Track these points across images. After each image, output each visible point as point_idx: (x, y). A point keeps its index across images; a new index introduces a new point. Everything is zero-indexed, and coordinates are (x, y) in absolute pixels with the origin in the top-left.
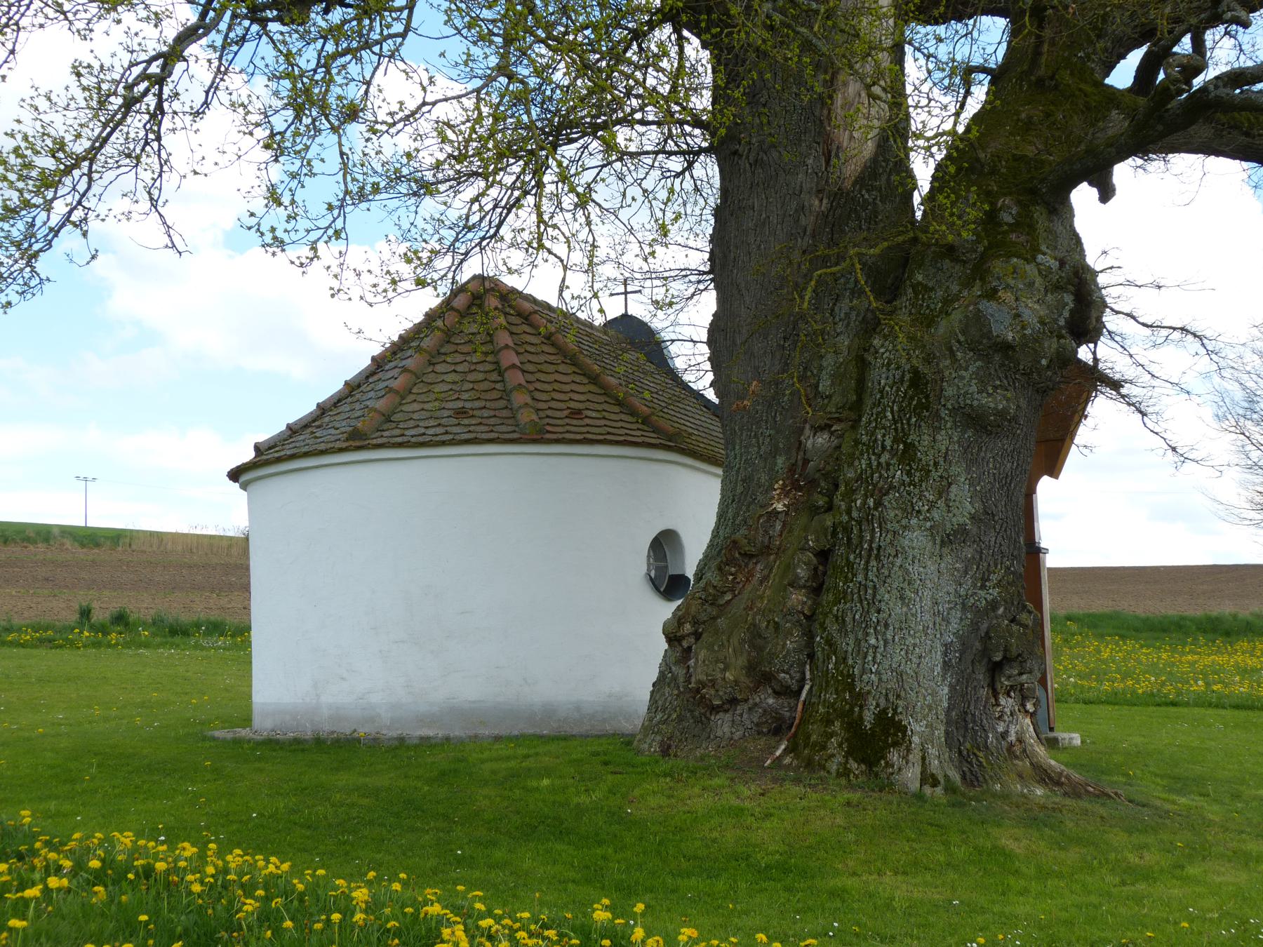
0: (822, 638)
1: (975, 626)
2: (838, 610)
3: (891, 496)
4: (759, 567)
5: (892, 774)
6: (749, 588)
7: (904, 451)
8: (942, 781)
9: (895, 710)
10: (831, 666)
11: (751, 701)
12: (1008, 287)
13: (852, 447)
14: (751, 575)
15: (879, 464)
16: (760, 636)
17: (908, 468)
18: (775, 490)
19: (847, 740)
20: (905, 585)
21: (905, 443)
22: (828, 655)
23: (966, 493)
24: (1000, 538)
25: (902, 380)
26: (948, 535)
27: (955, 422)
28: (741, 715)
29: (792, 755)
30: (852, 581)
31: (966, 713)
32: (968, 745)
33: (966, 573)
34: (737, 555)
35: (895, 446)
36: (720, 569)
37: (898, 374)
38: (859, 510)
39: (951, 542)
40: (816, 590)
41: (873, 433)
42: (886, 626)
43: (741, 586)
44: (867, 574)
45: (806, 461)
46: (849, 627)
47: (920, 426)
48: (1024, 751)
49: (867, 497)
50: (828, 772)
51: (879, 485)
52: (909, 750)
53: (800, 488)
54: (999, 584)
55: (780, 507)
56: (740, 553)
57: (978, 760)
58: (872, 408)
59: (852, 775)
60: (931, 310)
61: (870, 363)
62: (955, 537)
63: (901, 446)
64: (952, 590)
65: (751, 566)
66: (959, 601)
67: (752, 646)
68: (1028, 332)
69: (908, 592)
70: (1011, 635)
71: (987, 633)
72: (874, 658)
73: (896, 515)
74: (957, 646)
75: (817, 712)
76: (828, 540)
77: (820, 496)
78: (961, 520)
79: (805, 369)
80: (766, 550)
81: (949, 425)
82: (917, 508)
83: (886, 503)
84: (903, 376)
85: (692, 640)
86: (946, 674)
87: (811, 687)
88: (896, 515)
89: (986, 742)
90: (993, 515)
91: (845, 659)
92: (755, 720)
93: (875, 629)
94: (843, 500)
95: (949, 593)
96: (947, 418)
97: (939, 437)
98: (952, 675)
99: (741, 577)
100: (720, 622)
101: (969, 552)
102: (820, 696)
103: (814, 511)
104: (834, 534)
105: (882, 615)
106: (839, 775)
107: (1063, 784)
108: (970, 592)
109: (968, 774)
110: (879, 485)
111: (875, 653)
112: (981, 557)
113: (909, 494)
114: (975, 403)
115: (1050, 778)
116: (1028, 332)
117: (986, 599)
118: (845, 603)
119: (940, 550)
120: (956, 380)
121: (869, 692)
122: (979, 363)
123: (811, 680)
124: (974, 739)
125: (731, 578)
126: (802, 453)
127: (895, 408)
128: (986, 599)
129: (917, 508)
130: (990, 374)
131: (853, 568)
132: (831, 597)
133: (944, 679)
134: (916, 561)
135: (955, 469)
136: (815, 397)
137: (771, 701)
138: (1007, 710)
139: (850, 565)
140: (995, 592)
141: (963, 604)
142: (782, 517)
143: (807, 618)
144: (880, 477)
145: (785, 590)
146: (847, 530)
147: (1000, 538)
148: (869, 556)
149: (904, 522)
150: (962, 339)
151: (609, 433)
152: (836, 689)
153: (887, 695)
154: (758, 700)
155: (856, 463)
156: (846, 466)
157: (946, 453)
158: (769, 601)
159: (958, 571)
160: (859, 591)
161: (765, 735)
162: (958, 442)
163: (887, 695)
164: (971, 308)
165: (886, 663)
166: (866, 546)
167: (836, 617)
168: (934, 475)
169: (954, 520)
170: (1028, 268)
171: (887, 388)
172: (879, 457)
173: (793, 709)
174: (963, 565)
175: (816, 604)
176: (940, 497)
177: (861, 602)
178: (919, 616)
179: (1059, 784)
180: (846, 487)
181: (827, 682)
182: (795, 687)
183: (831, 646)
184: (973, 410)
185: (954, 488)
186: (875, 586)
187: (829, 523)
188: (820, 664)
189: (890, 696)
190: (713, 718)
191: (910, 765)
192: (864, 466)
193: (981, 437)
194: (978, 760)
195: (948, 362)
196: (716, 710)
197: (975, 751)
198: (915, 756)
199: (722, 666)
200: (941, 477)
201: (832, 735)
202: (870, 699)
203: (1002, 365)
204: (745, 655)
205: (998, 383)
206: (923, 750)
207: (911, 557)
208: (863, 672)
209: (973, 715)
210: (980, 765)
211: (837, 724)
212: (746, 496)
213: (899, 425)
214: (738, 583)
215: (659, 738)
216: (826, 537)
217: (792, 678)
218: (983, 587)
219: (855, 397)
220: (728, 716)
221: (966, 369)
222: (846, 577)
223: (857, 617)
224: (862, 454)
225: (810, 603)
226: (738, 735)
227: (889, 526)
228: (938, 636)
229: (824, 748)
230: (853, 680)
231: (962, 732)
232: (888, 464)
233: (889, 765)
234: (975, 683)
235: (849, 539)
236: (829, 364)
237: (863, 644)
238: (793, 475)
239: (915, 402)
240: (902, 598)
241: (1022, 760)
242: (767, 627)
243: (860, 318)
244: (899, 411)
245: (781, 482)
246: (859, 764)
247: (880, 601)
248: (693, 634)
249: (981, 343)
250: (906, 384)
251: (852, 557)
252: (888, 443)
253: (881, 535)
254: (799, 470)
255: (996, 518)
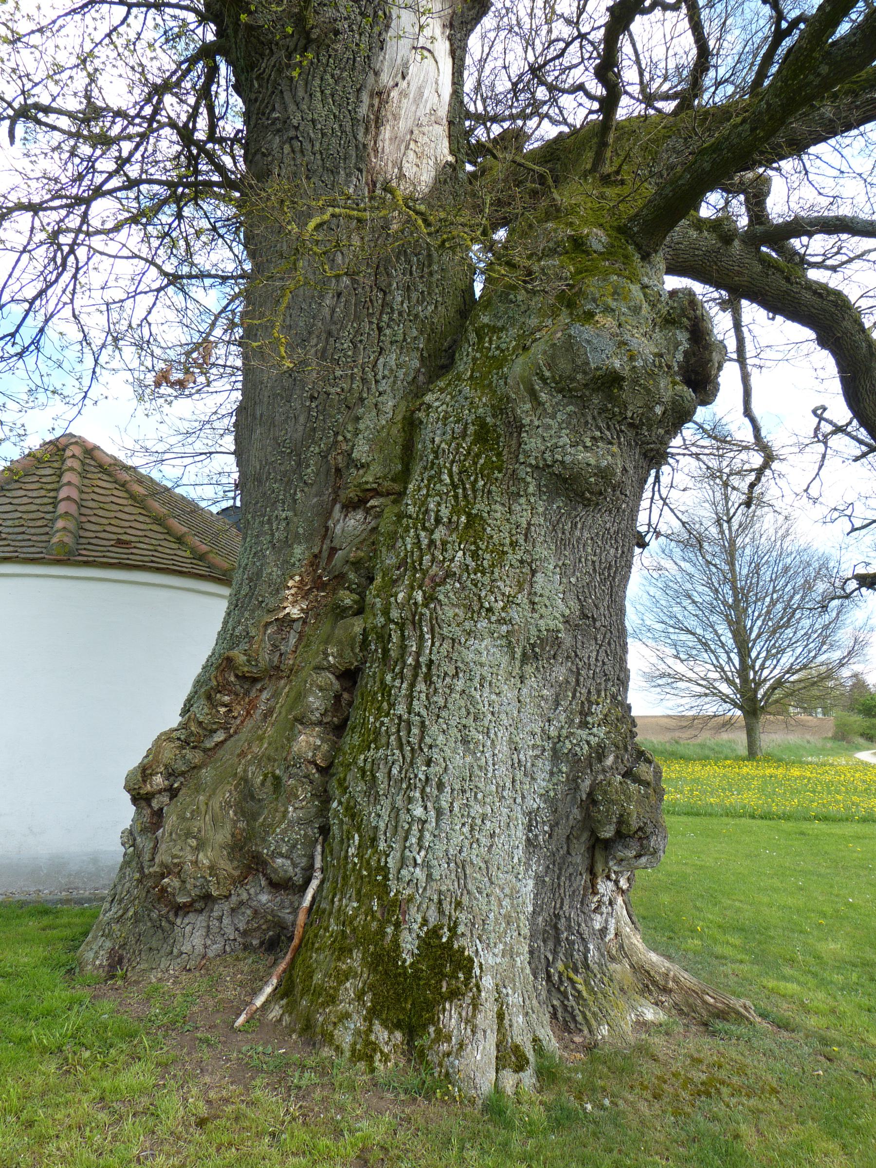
0: (340, 803)
1: (573, 782)
2: (365, 760)
3: (448, 586)
4: (265, 695)
5: (448, 1054)
6: (249, 724)
7: (468, 525)
8: (531, 1055)
9: (453, 929)
10: (352, 851)
11: (234, 899)
12: (608, 310)
13: (394, 523)
14: (252, 706)
15: (432, 542)
16: (253, 797)
17: (473, 548)
18: (289, 588)
19: (372, 987)
20: (470, 721)
21: (469, 515)
22: (349, 832)
23: (557, 586)
24: (602, 655)
25: (464, 435)
26: (533, 646)
27: (539, 486)
28: (220, 919)
29: (283, 1002)
30: (387, 714)
31: (557, 916)
32: (560, 966)
33: (557, 704)
34: (232, 679)
35: (455, 518)
36: (209, 698)
37: (458, 429)
38: (401, 607)
39: (536, 657)
40: (339, 729)
41: (424, 503)
42: (440, 786)
43: (238, 722)
44: (411, 704)
45: (333, 550)
46: (382, 787)
47: (490, 492)
48: (621, 947)
49: (412, 588)
50: (338, 1049)
51: (432, 572)
52: (475, 1005)
53: (322, 586)
54: (605, 721)
55: (295, 612)
56: (237, 676)
57: (574, 988)
58: (422, 474)
59: (378, 1056)
60: (502, 351)
61: (421, 422)
62: (543, 649)
63: (463, 519)
64: (538, 730)
65: (253, 694)
66: (548, 746)
67: (242, 812)
68: (639, 363)
69: (474, 732)
70: (629, 798)
71: (590, 794)
72: (420, 839)
73: (456, 615)
74: (545, 814)
75: (326, 929)
76: (355, 654)
77: (347, 592)
78: (552, 624)
79: (336, 434)
80: (275, 672)
81: (531, 489)
82: (487, 605)
83: (441, 597)
84: (465, 428)
85: (166, 799)
86: (529, 859)
87: (322, 882)
88: (456, 615)
89: (586, 958)
90: (594, 620)
91: (374, 840)
92: (242, 926)
93: (423, 791)
94: (378, 596)
95: (533, 734)
96: (529, 479)
97: (516, 508)
98: (539, 859)
99: (238, 710)
100: (206, 774)
101: (560, 672)
102: (333, 902)
103: (340, 613)
104: (365, 644)
105: (434, 769)
106: (356, 1056)
107: (671, 991)
108: (564, 732)
109: (560, 1010)
110: (432, 572)
111: (421, 831)
112: (577, 681)
113: (476, 585)
114: (568, 459)
115: (655, 983)
116: (639, 363)
117: (588, 743)
118: (377, 748)
119: (520, 668)
120: (540, 430)
121: (410, 899)
122: (570, 408)
123: (322, 870)
124: (569, 955)
125: (223, 710)
126: (327, 542)
127: (455, 469)
128: (588, 743)
129: (487, 605)
130: (587, 423)
131: (390, 695)
132: (356, 739)
133: (528, 866)
134: (486, 685)
135: (542, 551)
136: (347, 467)
137: (264, 898)
138: (606, 899)
139: (385, 689)
140: (601, 731)
141: (554, 750)
142: (298, 626)
143: (325, 771)
144: (433, 561)
145: (292, 728)
146: (384, 638)
147: (602, 655)
148: (415, 676)
149: (468, 625)
150: (547, 374)
151: (152, 562)
152: (359, 892)
153: (440, 902)
154: (245, 896)
155: (399, 543)
156: (384, 550)
157: (528, 529)
158: (270, 744)
159: (546, 700)
160: (399, 731)
161: (254, 950)
162: (544, 514)
163: (440, 902)
164: (559, 335)
165: (440, 848)
166: (410, 661)
167: (363, 771)
168: (513, 558)
169: (541, 622)
170: (632, 287)
171: (443, 445)
172: (432, 532)
173: (295, 911)
174: (552, 691)
175: (336, 749)
176: (521, 589)
177: (401, 747)
178: (491, 769)
179: (665, 990)
180: (383, 578)
181: (345, 878)
182: (298, 880)
183: (353, 817)
184: (565, 468)
185: (539, 578)
186: (423, 723)
187: (358, 629)
188: (336, 845)
189: (446, 906)
190: (179, 921)
191: (479, 1035)
192: (409, 547)
193: (575, 509)
194: (574, 988)
195: (528, 406)
196: (180, 910)
197: (572, 975)
198: (486, 1018)
199: (193, 842)
200: (522, 562)
201: (347, 975)
202: (413, 910)
203: (603, 410)
204: (228, 826)
205: (598, 434)
206: (500, 1000)
207: (478, 678)
208: (402, 863)
209: (568, 919)
210: (579, 996)
211: (357, 955)
212: (251, 597)
213: (460, 491)
214: (235, 718)
215: (108, 944)
216: (352, 650)
217: (294, 865)
218: (584, 725)
219: (400, 467)
220: (200, 920)
221: (553, 417)
222: (379, 709)
223: (395, 771)
224: (407, 530)
225: (325, 747)
226: (216, 948)
227: (445, 631)
228: (519, 800)
229: (333, 1000)
230: (386, 878)
231: (551, 945)
232: (444, 543)
233: (442, 1036)
234: (571, 870)
235: (386, 651)
236: (367, 427)
237: (404, 816)
238: (315, 571)
239: (482, 461)
240: (465, 741)
241: (620, 962)
242: (263, 783)
243: (410, 378)
244: (460, 473)
245: (297, 578)
246: (391, 1033)
247: (431, 747)
248: (165, 790)
249: (573, 379)
250: (469, 440)
251: (388, 678)
252: (445, 512)
253: (433, 644)
254: (323, 564)
255: (598, 624)
